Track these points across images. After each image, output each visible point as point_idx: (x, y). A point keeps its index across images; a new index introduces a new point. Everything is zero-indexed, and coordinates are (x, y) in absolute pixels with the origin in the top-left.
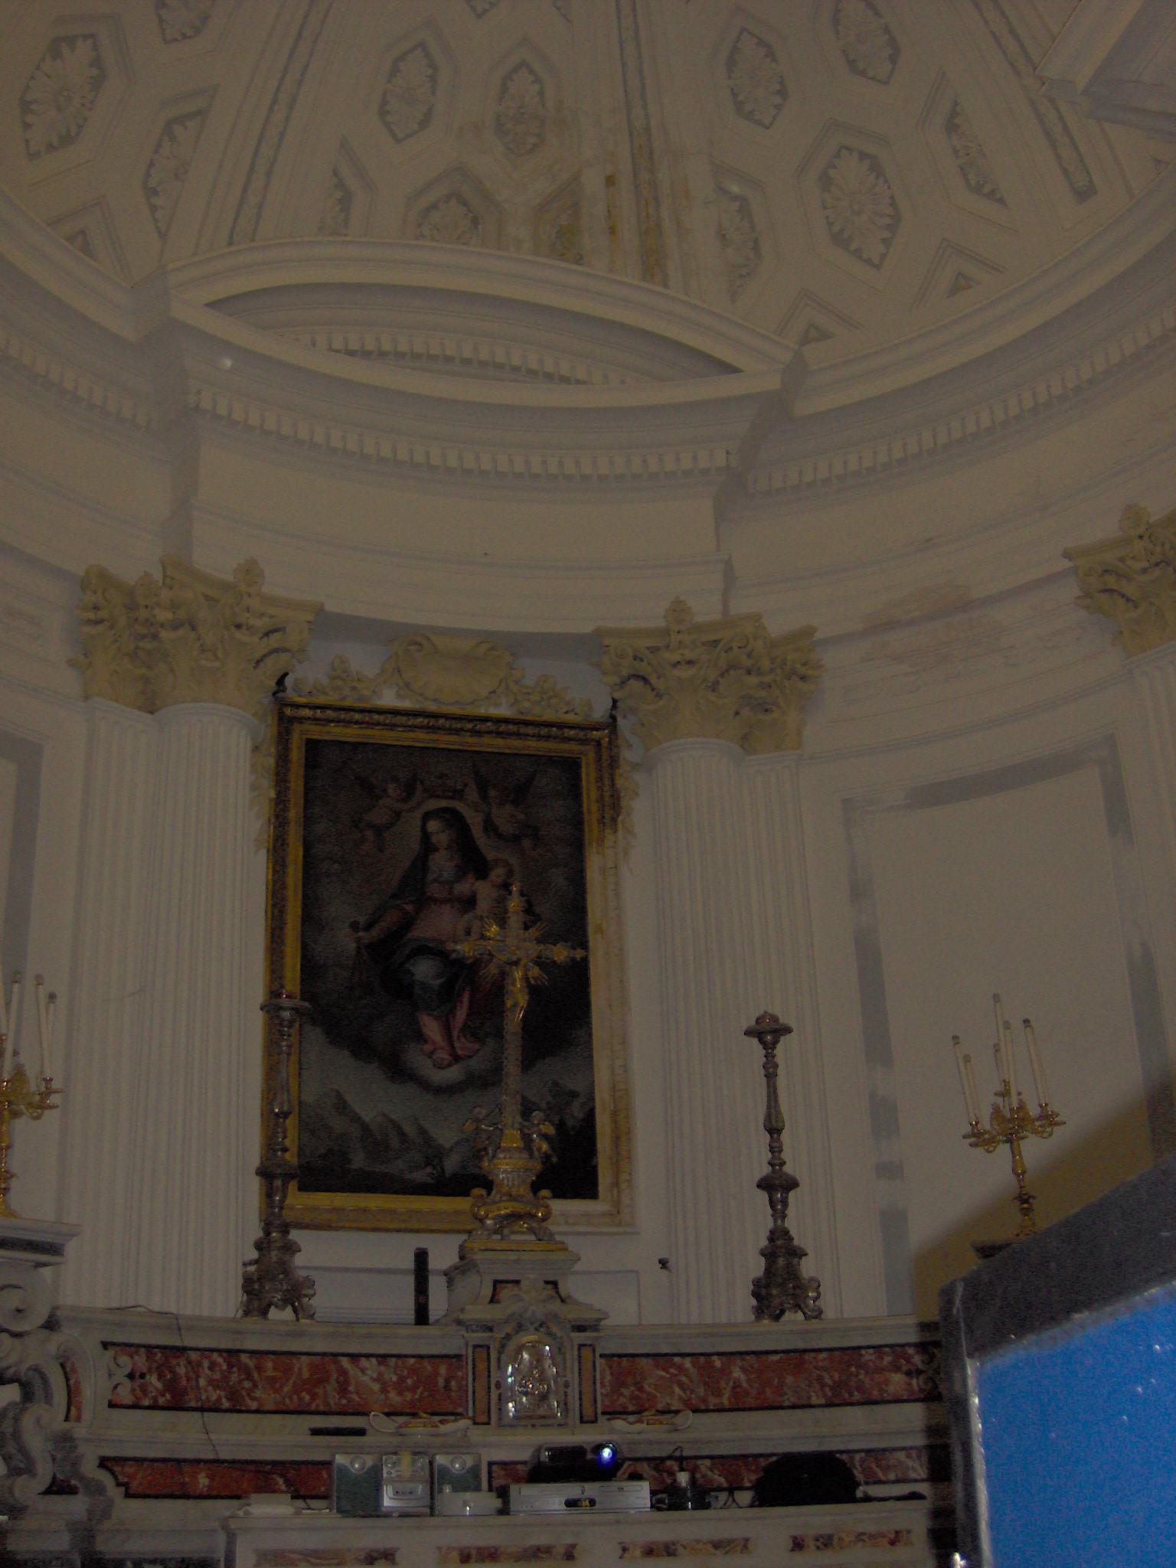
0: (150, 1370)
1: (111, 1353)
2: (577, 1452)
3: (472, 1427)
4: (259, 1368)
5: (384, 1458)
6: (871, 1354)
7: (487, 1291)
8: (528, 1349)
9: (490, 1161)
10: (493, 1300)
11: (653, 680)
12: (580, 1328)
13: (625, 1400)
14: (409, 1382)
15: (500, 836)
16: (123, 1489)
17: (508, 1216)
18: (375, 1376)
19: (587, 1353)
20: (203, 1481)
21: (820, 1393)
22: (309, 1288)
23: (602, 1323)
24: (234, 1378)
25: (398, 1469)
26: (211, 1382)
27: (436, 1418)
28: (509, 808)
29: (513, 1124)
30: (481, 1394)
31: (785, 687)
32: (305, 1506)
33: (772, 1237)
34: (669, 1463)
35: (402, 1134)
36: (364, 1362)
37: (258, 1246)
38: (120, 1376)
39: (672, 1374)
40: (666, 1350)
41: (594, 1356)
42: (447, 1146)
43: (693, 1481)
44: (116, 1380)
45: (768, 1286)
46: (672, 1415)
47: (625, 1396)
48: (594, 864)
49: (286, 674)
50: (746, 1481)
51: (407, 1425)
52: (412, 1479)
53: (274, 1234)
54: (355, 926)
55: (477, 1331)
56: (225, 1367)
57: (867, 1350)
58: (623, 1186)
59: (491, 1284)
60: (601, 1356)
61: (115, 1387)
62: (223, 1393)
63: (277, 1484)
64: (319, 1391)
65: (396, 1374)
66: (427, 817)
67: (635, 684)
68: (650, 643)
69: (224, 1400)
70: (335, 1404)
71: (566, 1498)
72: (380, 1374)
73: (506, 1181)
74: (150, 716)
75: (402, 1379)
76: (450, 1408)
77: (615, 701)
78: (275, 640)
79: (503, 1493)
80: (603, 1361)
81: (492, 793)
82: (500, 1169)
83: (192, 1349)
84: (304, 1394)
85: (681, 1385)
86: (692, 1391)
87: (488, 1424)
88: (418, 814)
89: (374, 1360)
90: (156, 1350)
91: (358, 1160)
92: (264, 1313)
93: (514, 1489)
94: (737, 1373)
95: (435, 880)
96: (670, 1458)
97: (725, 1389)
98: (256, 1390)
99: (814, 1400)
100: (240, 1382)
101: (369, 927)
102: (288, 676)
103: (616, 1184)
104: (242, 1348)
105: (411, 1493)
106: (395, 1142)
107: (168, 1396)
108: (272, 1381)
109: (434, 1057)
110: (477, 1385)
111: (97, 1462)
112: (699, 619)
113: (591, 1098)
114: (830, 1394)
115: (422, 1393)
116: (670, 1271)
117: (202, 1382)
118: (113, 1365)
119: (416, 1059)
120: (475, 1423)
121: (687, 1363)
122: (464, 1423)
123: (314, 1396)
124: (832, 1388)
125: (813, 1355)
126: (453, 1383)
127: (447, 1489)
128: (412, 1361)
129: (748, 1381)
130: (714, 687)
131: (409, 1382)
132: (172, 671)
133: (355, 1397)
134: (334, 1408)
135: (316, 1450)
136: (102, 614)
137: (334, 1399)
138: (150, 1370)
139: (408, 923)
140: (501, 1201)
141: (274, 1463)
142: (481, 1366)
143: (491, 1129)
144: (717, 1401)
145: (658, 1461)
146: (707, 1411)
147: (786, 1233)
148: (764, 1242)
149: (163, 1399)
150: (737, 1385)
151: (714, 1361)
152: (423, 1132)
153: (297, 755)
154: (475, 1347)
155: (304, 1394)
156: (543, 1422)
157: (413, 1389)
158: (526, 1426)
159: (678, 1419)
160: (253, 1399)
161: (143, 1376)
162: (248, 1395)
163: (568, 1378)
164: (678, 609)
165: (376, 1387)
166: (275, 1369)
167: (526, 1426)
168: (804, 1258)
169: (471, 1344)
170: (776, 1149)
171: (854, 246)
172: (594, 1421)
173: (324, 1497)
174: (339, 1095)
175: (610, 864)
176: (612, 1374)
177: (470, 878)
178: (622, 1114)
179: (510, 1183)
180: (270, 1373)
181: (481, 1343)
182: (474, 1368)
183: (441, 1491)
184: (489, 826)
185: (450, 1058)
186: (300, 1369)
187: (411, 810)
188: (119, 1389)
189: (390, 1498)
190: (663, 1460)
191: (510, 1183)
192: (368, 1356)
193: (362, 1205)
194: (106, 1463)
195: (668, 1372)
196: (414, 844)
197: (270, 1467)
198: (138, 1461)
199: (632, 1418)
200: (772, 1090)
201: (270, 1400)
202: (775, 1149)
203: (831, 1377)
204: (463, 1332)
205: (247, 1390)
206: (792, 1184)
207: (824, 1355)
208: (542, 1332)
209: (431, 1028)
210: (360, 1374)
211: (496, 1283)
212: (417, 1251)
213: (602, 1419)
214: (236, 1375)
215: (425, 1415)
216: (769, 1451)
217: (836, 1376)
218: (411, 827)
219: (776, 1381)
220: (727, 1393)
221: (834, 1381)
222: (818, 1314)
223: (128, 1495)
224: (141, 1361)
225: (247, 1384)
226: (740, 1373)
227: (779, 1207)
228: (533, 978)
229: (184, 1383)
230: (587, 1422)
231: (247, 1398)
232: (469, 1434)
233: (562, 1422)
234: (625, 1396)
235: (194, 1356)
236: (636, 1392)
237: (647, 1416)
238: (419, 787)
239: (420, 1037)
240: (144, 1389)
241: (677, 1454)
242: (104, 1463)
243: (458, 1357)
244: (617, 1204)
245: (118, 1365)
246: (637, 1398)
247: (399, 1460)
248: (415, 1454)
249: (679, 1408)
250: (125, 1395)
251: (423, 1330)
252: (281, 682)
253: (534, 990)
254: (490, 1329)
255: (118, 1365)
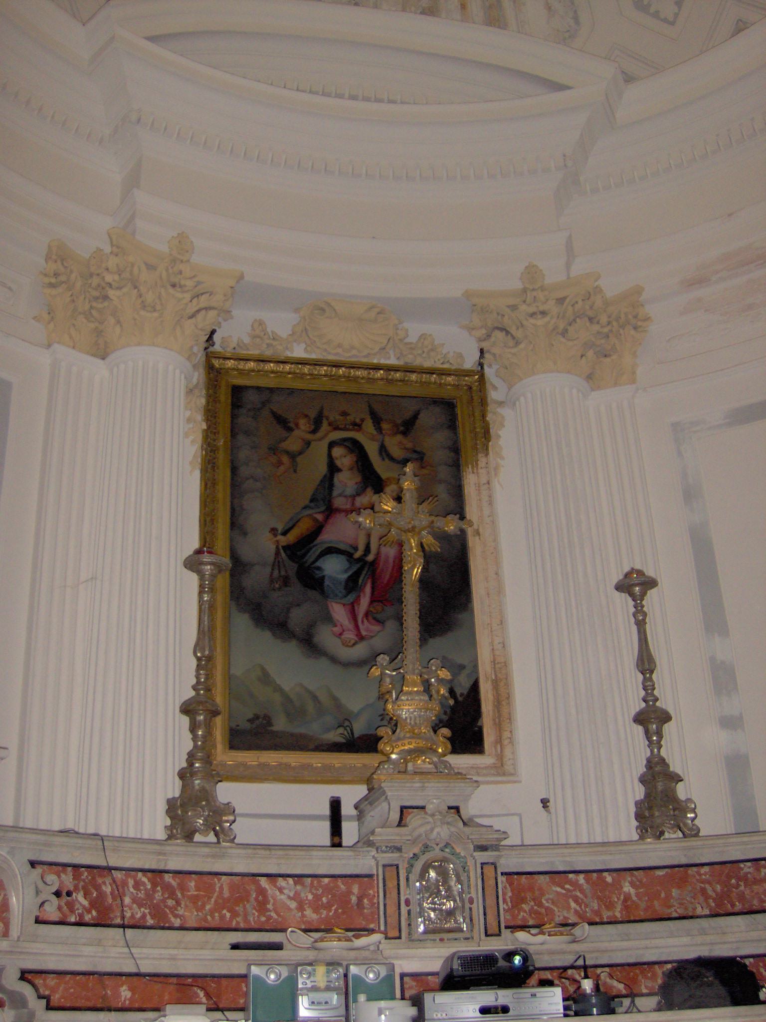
0: (76, 888)
1: (39, 870)
2: (489, 959)
3: (383, 941)
4: (183, 888)
5: (299, 969)
6: (749, 867)
7: (395, 816)
8: (434, 868)
9: (394, 703)
10: (401, 823)
11: (513, 330)
12: (483, 848)
13: (525, 915)
14: (324, 900)
15: (392, 459)
16: (44, 1001)
17: (410, 752)
18: (292, 894)
19: (489, 871)
20: (125, 993)
21: (704, 905)
22: (230, 814)
23: (503, 843)
24: (158, 896)
25: (312, 979)
26: (134, 900)
27: (350, 934)
28: (399, 437)
29: (414, 670)
30: (392, 910)
31: (620, 335)
32: (224, 1018)
33: (650, 764)
34: (570, 972)
35: (315, 698)
36: (281, 882)
37: (182, 775)
38: (47, 893)
39: (568, 890)
40: (561, 868)
41: (496, 873)
42: (356, 711)
43: (597, 988)
44: (43, 897)
45: (650, 808)
46: (570, 928)
47: (525, 911)
48: (470, 481)
49: (213, 332)
50: (643, 987)
51: (322, 940)
52: (328, 989)
53: (197, 765)
54: (274, 531)
55: (385, 852)
56: (149, 887)
57: (745, 863)
58: (506, 742)
59: (399, 810)
60: (502, 874)
61: (42, 904)
62: (147, 911)
63: (198, 996)
64: (239, 909)
65: (312, 894)
66: (332, 445)
67: (499, 335)
68: (511, 301)
69: (148, 917)
70: (255, 922)
71: (481, 1005)
72: (297, 894)
73: (408, 721)
74: (101, 362)
75: (317, 898)
76: (364, 924)
77: (482, 351)
78: (204, 301)
79: (417, 1002)
80: (504, 878)
81: (385, 426)
82: (403, 709)
83: (116, 869)
84: (225, 911)
85: (576, 900)
86: (586, 906)
87: (400, 938)
88: (325, 444)
89: (291, 880)
90: (83, 869)
91: (280, 724)
92: (189, 837)
93: (428, 997)
94: (627, 888)
95: (340, 495)
96: (572, 967)
97: (616, 902)
98: (179, 908)
99: (699, 911)
100: (164, 901)
101: (285, 533)
102: (216, 334)
103: (499, 741)
104: (167, 868)
105: (326, 1003)
106: (310, 707)
107: (94, 913)
108: (194, 899)
109: (343, 637)
110: (388, 901)
111: (19, 975)
112: (548, 281)
113: (476, 667)
114: (713, 904)
115: (336, 910)
116: (549, 812)
117: (127, 900)
118: (41, 885)
119: (325, 637)
120: (386, 938)
121: (581, 878)
122: (376, 937)
123: (234, 914)
124: (714, 900)
125: (695, 869)
126: (365, 901)
127: (362, 998)
128: (326, 880)
129: (637, 895)
130: (564, 333)
131: (324, 900)
132: (119, 322)
133: (273, 914)
134: (253, 925)
135: (236, 962)
136: (63, 278)
137: (254, 917)
138: (76, 888)
139: (318, 530)
140: (404, 738)
141: (194, 976)
142: (391, 884)
143: (394, 673)
144: (610, 913)
145: (562, 970)
146: (602, 923)
147: (663, 761)
148: (642, 769)
149: (90, 916)
150: (627, 898)
151: (606, 878)
152: (335, 699)
153: (224, 396)
154: (384, 866)
155: (225, 911)
156: (451, 935)
157: (328, 907)
158: (434, 940)
159: (577, 931)
160: (176, 916)
161: (69, 894)
162: (172, 913)
163: (473, 895)
164: (532, 273)
165: (293, 905)
166: (198, 888)
167: (434, 940)
168: (680, 783)
169: (380, 864)
170: (649, 688)
171: (652, 10)
172: (499, 934)
173: (242, 1009)
174: (263, 670)
175: (484, 480)
176: (512, 891)
177: (369, 491)
178: (502, 683)
179: (413, 723)
180: (193, 892)
181: (391, 862)
182: (384, 886)
183: (355, 1001)
184: (383, 451)
185: (356, 638)
186: (221, 888)
187: (320, 439)
188: (46, 905)
189: (306, 1008)
190: (565, 969)
191: (413, 723)
192: (285, 876)
193: (285, 760)
194: (26, 975)
195: (563, 888)
196: (323, 469)
197: (190, 980)
198: (60, 973)
199: (533, 931)
200: (643, 637)
201: (192, 917)
202: (648, 687)
203: (714, 891)
204: (373, 852)
205: (171, 908)
206: (666, 717)
207: (706, 869)
208: (447, 852)
209: (339, 612)
210: (278, 893)
211: (403, 808)
212: (332, 799)
213: (506, 933)
214: (160, 894)
215: (339, 931)
216: (663, 958)
217: (718, 888)
218: (319, 450)
219: (663, 895)
220: (619, 907)
221: (717, 894)
222: (694, 833)
223: (49, 1008)
224: (68, 880)
225: (170, 902)
226: (630, 888)
227: (655, 738)
228: (427, 545)
229: (110, 900)
230: (491, 935)
231: (170, 916)
232: (381, 947)
233: (468, 936)
234: (525, 911)
235: (118, 875)
236: (535, 907)
237: (548, 928)
238: (325, 423)
239: (328, 619)
240: (71, 906)
241: (580, 962)
242: (25, 975)
243: (370, 876)
244: (500, 757)
245: (45, 883)
246: (538, 913)
247: (314, 970)
248: (329, 964)
249: (576, 921)
250: (52, 911)
251: (337, 852)
252: (210, 338)
253: (428, 557)
254: (399, 849)
255: (45, 883)
